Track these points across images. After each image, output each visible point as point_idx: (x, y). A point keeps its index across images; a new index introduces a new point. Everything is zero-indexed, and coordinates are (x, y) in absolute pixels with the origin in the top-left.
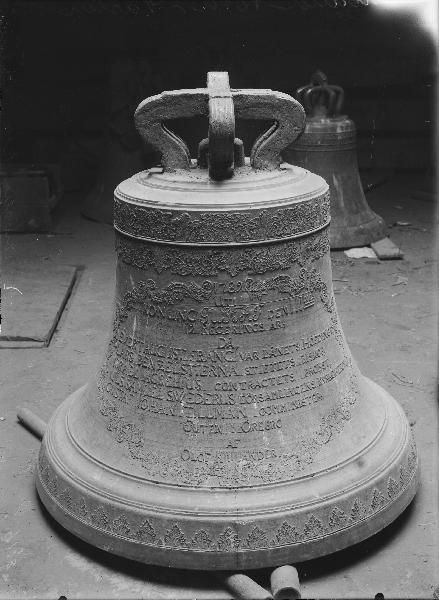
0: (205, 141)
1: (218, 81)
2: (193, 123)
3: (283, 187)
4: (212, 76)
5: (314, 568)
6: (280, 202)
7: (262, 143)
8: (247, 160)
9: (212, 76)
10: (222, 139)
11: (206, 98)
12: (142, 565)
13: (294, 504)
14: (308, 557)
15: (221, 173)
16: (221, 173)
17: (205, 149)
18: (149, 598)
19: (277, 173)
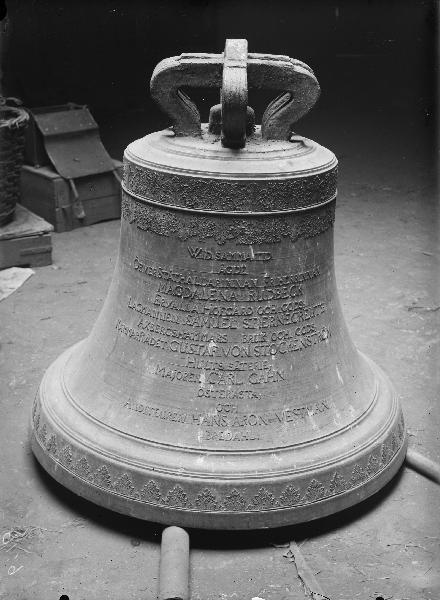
0: (218, 107)
1: (237, 47)
2: (204, 87)
3: (184, 158)
4: (230, 43)
5: (205, 539)
6: (294, 174)
7: (275, 110)
8: (258, 128)
9: (230, 43)
10: (234, 105)
11: (219, 68)
12: (299, 539)
13: (248, 474)
14: (207, 525)
15: (234, 142)
16: (234, 142)
17: (217, 115)
18: (130, 598)
19: (286, 145)
